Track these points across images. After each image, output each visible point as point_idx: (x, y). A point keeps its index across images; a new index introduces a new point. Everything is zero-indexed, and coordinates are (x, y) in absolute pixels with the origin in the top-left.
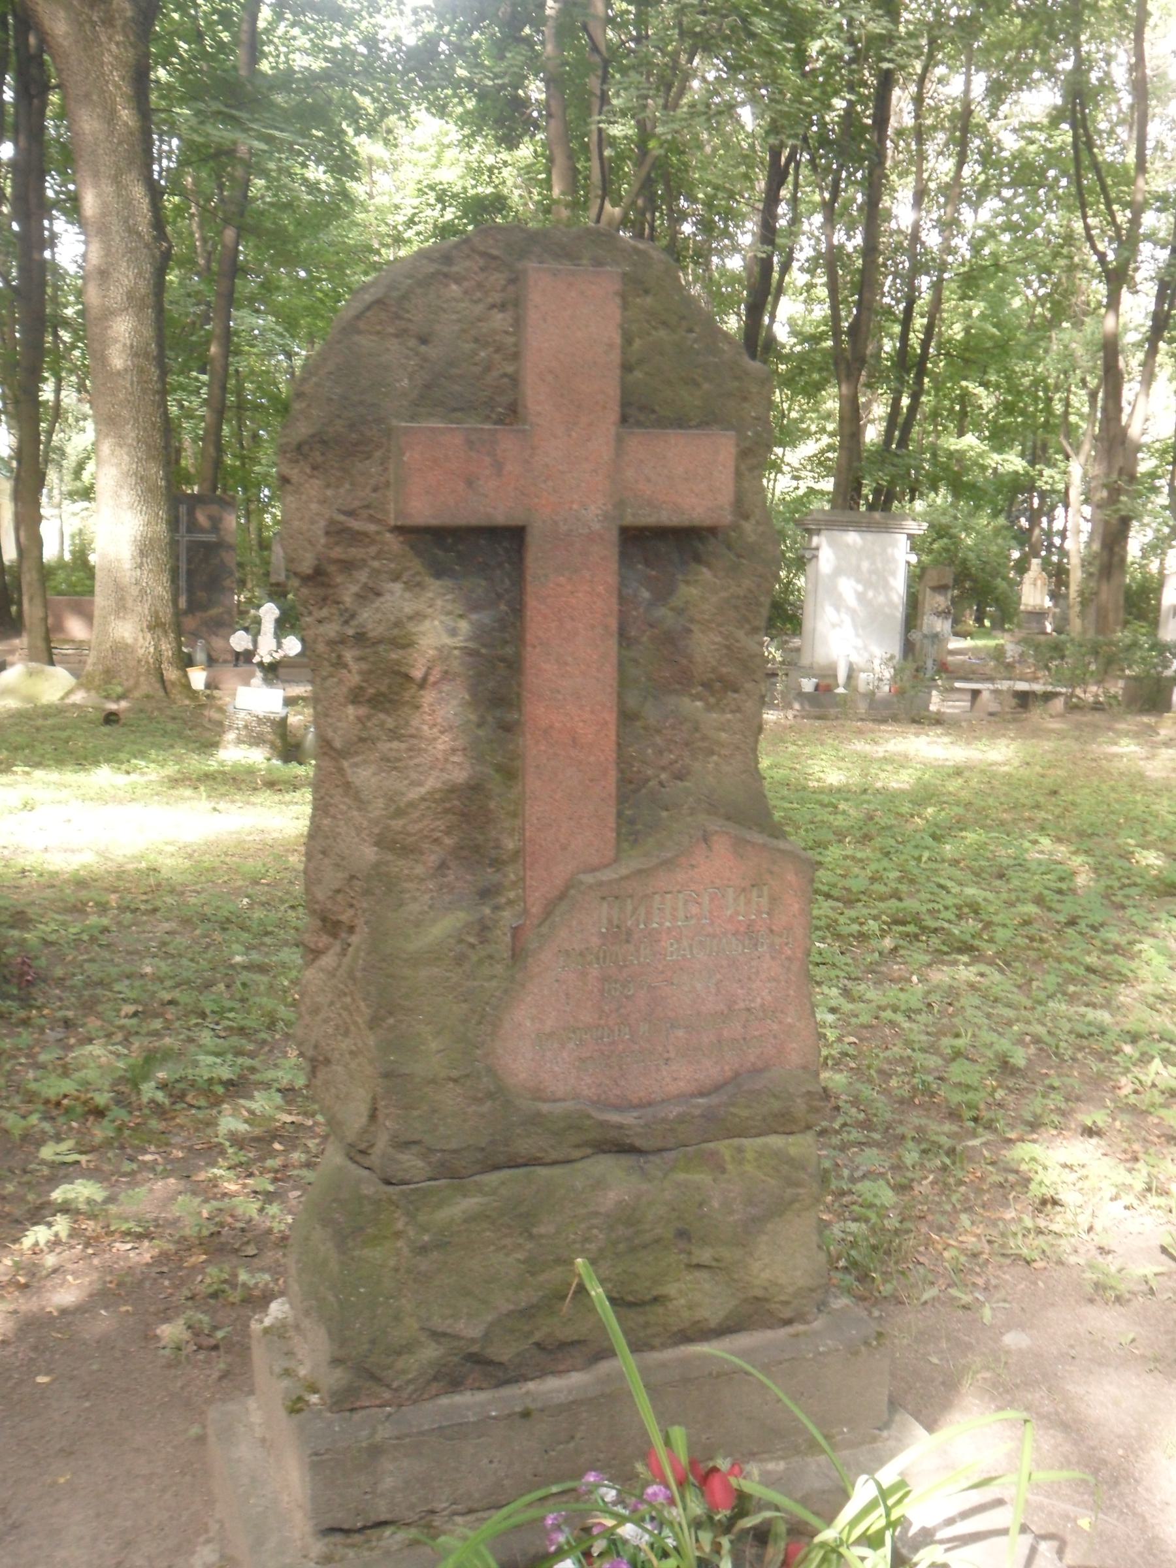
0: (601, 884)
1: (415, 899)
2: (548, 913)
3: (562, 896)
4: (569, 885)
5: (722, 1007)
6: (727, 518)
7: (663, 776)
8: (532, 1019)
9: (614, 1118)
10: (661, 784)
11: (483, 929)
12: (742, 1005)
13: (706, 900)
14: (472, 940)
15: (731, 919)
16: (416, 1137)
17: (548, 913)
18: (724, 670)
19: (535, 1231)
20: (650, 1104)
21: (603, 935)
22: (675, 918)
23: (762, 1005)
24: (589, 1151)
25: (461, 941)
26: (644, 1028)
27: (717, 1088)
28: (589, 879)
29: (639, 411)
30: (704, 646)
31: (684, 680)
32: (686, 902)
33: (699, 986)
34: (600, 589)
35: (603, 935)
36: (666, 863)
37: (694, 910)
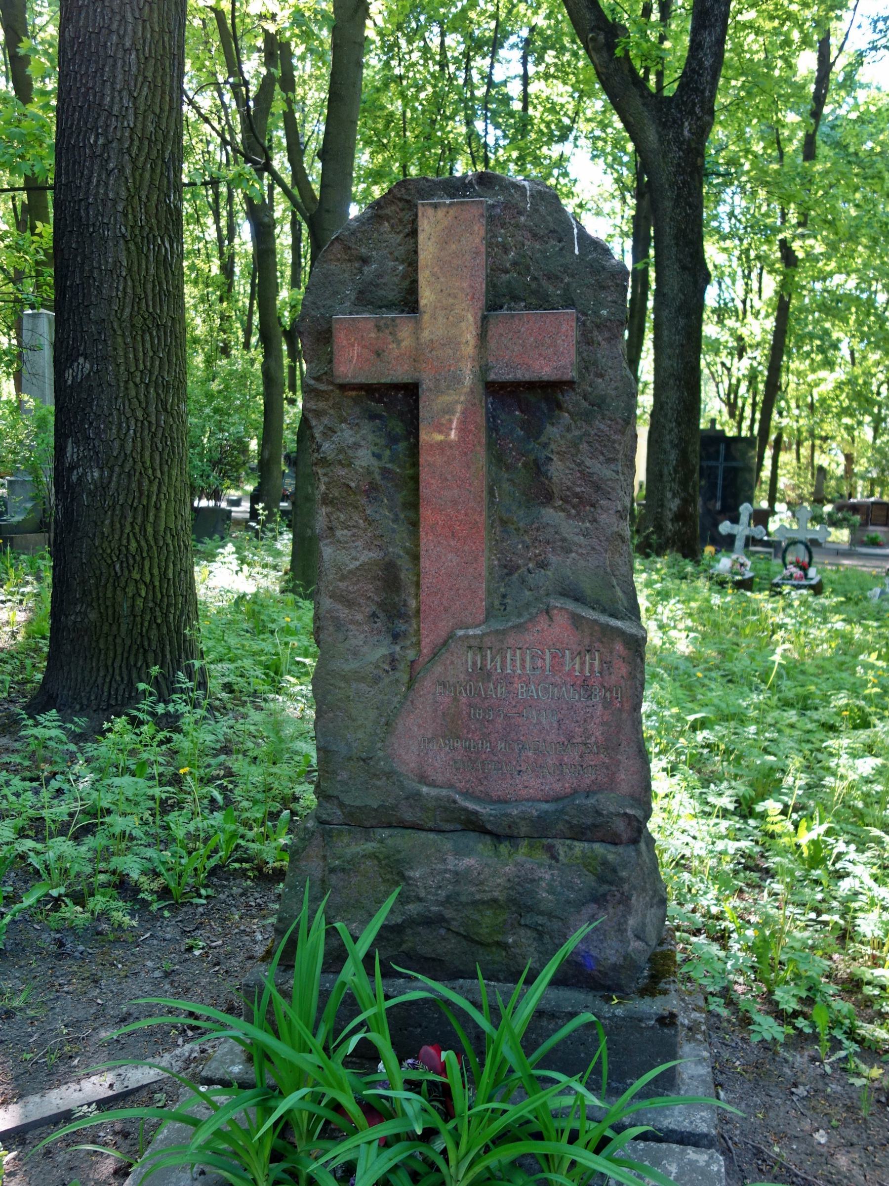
0: (468, 637)
1: (355, 637)
2: (435, 655)
3: (445, 643)
4: (451, 636)
5: (562, 738)
6: (571, 374)
7: (531, 565)
8: (419, 726)
9: (471, 806)
10: (529, 571)
11: (393, 661)
12: (579, 740)
13: (548, 656)
14: (387, 667)
15: (569, 674)
16: (336, 793)
17: (435, 655)
18: (578, 490)
19: (407, 873)
20: (506, 802)
21: (469, 674)
22: (523, 667)
23: (596, 743)
24: (459, 827)
25: (377, 667)
26: (501, 745)
27: (557, 799)
28: (461, 633)
29: (498, 299)
30: (559, 471)
31: (548, 497)
32: (532, 658)
33: (544, 721)
34: (472, 427)
35: (469, 674)
36: (518, 627)
37: (539, 663)
